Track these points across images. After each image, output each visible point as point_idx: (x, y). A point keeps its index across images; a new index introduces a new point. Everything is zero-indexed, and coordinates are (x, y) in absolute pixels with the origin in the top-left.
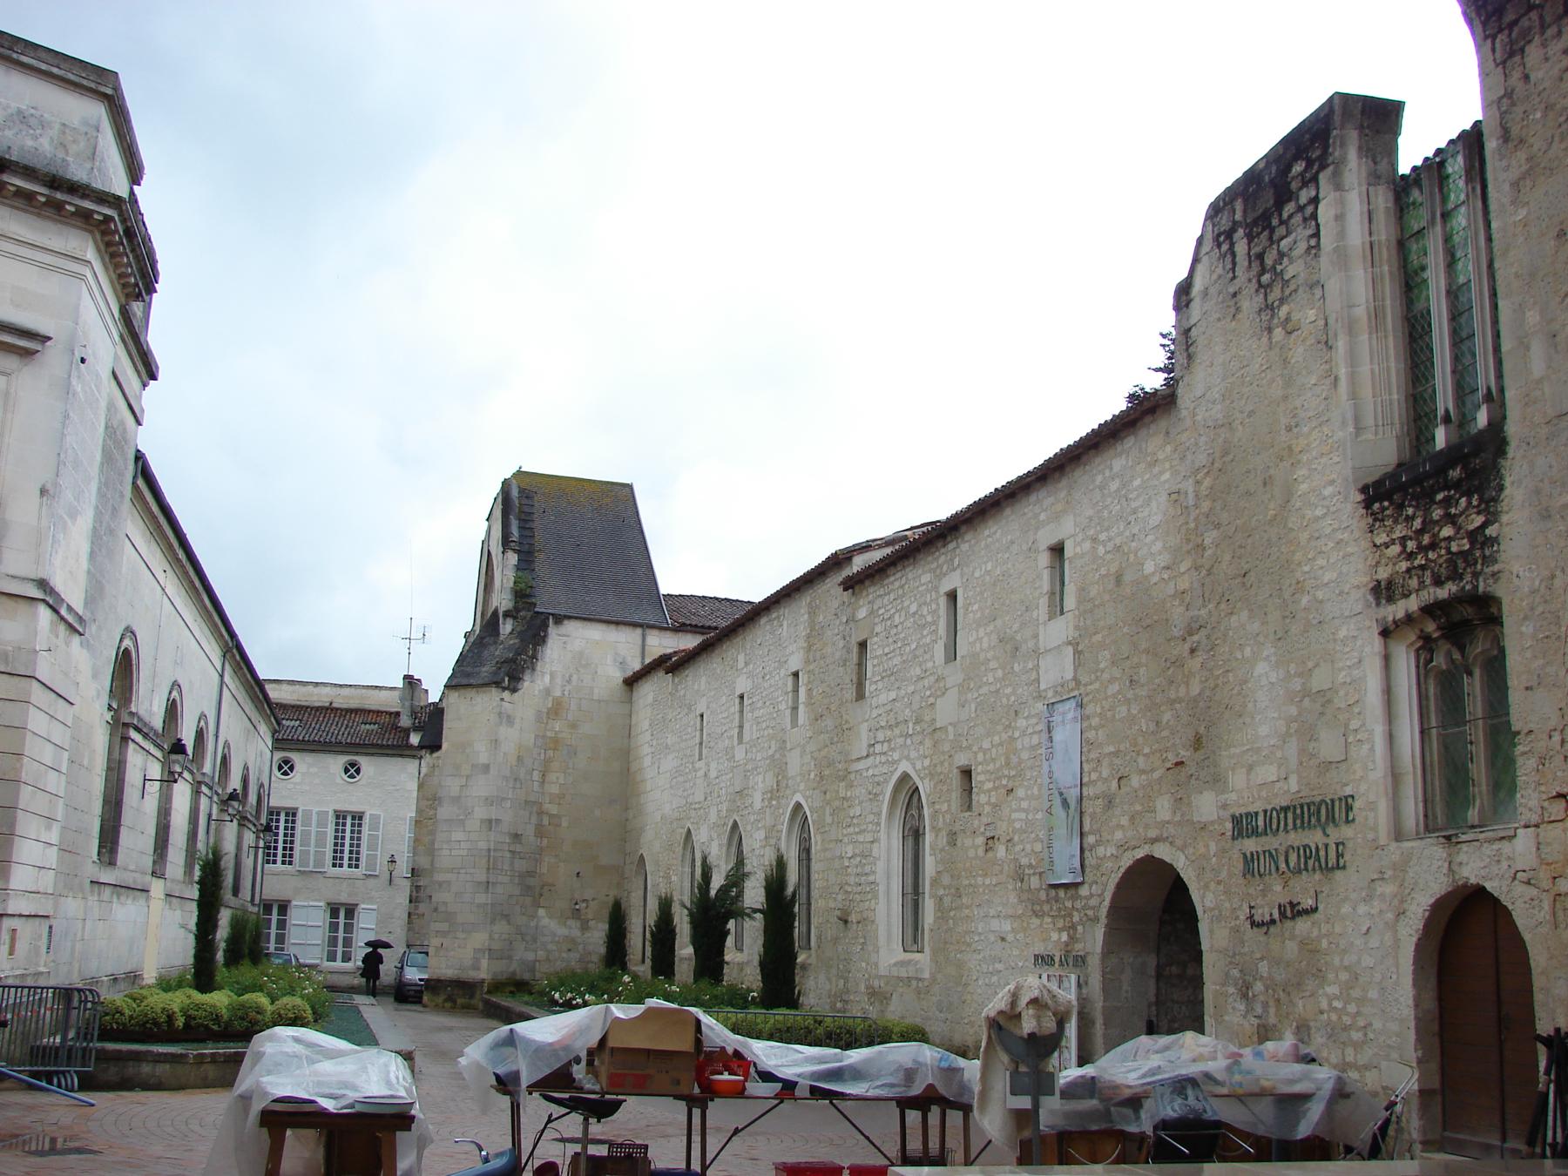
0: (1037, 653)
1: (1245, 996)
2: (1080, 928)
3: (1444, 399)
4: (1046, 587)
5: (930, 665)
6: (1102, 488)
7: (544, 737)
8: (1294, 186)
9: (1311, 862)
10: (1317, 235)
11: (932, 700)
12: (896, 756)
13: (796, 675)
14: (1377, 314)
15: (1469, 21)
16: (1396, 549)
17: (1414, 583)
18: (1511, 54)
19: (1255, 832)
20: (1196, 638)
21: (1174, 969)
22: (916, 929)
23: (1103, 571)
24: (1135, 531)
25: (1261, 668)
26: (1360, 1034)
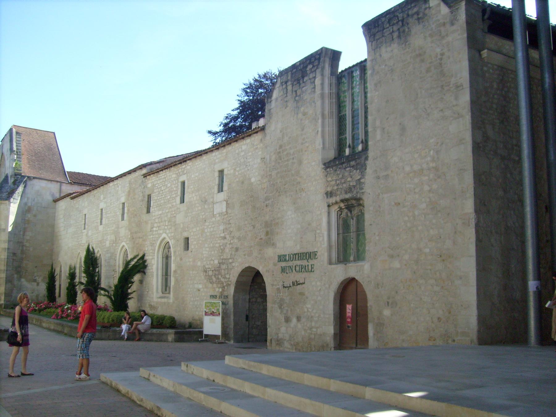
0: (213, 203)
1: (280, 308)
2: (226, 287)
3: (349, 141)
4: (217, 182)
5: (174, 204)
6: (238, 154)
7: (25, 219)
8: (308, 72)
9: (303, 270)
10: (314, 88)
11: (175, 215)
12: (161, 232)
13: (124, 204)
14: (332, 113)
15: (365, 36)
16: (334, 183)
17: (339, 193)
18: (377, 48)
19: (285, 260)
20: (268, 202)
21: (254, 300)
22: (166, 286)
23: (237, 180)
24: (249, 168)
25: (289, 213)
26: (317, 319)
